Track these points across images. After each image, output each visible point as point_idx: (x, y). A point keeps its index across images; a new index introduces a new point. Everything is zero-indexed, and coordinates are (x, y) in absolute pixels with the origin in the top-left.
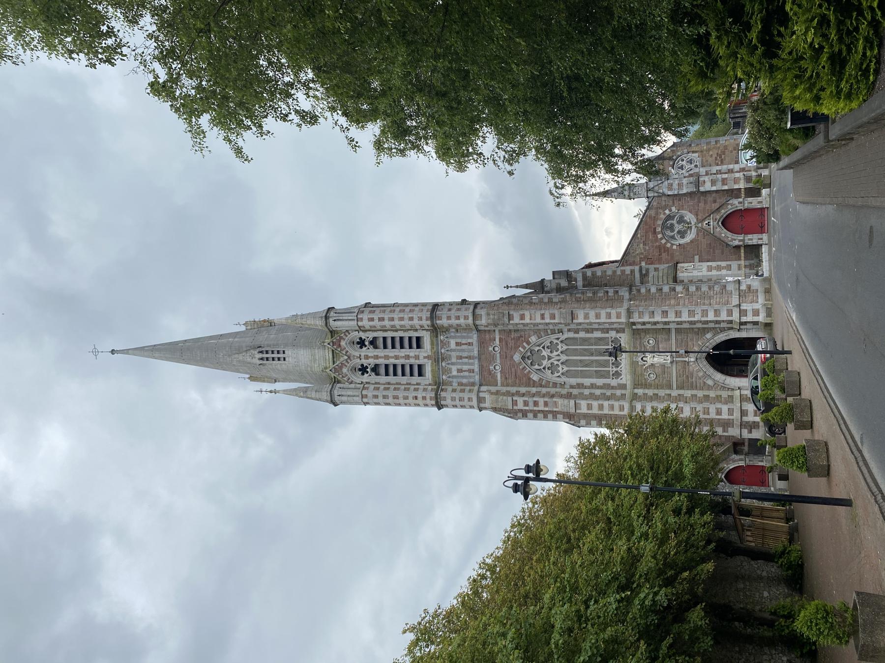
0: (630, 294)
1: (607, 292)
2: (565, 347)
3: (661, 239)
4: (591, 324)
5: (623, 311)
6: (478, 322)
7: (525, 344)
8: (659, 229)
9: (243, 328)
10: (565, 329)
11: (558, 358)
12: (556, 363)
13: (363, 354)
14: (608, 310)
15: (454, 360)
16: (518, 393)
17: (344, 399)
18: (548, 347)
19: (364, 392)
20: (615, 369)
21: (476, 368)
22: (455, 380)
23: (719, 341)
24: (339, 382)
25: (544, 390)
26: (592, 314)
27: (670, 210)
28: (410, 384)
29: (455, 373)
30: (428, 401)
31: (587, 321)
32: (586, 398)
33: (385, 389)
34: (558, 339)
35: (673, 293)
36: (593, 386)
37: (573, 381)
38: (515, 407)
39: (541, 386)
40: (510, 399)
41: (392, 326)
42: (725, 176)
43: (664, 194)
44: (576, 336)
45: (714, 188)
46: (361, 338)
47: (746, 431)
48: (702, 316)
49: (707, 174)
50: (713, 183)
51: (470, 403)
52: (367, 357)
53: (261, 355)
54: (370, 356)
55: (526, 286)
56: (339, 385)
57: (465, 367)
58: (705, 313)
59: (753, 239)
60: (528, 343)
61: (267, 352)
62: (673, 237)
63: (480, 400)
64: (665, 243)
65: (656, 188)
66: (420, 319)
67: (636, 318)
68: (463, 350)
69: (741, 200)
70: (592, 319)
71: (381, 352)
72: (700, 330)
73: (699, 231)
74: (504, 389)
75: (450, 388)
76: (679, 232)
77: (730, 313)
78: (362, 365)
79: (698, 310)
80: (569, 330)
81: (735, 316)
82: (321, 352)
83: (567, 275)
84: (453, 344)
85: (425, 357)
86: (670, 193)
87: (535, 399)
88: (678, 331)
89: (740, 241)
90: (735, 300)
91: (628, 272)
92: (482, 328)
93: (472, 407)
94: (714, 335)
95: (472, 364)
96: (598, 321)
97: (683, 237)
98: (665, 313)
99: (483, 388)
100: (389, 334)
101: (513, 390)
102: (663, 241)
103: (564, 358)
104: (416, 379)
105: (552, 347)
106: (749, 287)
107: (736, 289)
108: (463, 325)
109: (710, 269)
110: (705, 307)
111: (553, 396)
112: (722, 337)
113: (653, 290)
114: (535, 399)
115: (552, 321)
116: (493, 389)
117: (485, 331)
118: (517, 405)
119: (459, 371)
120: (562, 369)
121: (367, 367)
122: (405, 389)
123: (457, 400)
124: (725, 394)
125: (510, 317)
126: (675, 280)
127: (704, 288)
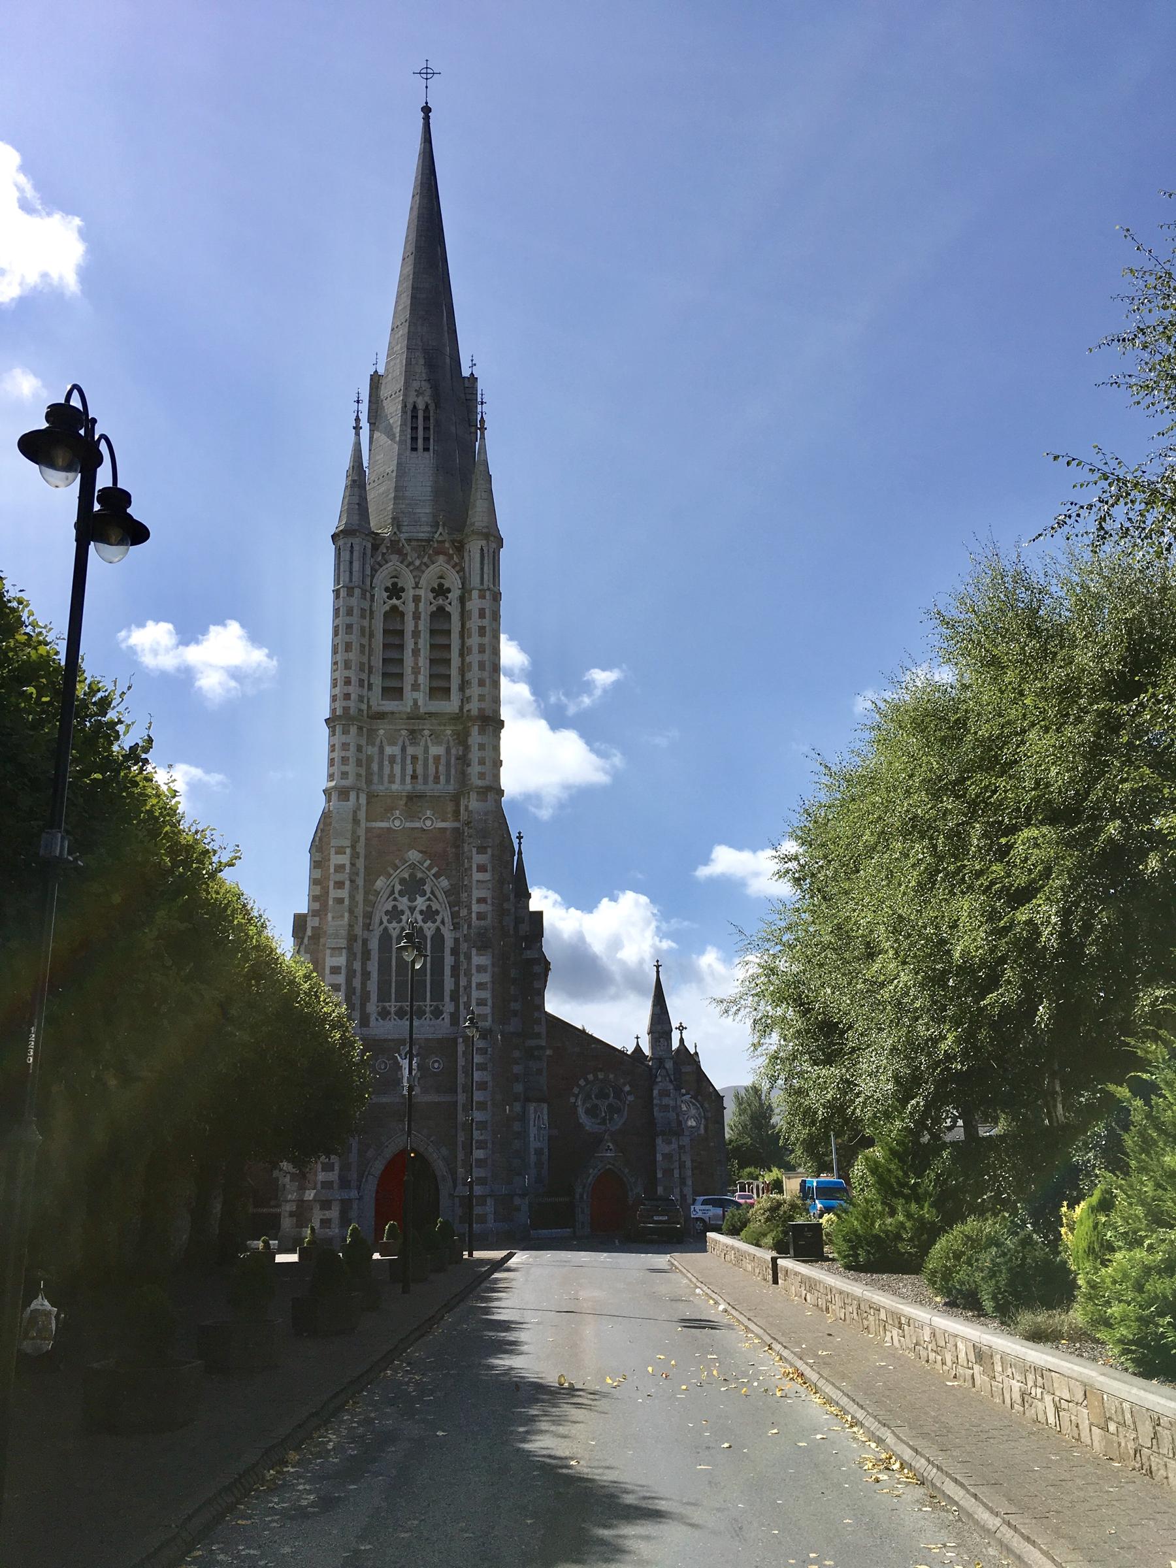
2: (429, 934)
3: (586, 1080)
4: (468, 974)
7: (428, 862)
9: (466, 373)
13: (422, 592)
14: (490, 1003)
16: (355, 856)
17: (346, 555)
18: (429, 907)
19: (357, 592)
20: (393, 1010)
22: (376, 749)
25: (360, 897)
26: (485, 978)
27: (629, 1093)
28: (370, 672)
29: (389, 750)
31: (474, 971)
33: (362, 629)
34: (443, 922)
36: (366, 975)
39: (366, 893)
40: (347, 843)
41: (470, 650)
42: (676, 1174)
43: (654, 1083)
44: (447, 951)
45: (659, 1157)
46: (449, 590)
47: (294, 1208)
49: (681, 1147)
50: (668, 1157)
52: (416, 599)
53: (421, 406)
60: (437, 876)
62: (588, 1097)
64: (579, 1086)
65: (664, 1072)
68: (426, 766)
75: (363, 742)
76: (596, 1106)
80: (456, 940)
85: (415, 702)
86: (655, 1092)
87: (347, 883)
89: (581, 1197)
91: (537, 1029)
92: (463, 802)
96: (474, 985)
97: (587, 1112)
102: (582, 1083)
108: (469, 770)
110: (490, 1145)
111: (351, 912)
113: (517, 1069)
115: (474, 916)
116: (362, 815)
118: (337, 853)
122: (362, 664)
123: (343, 754)
124: (353, 1176)
125: (482, 850)
126: (528, 1100)
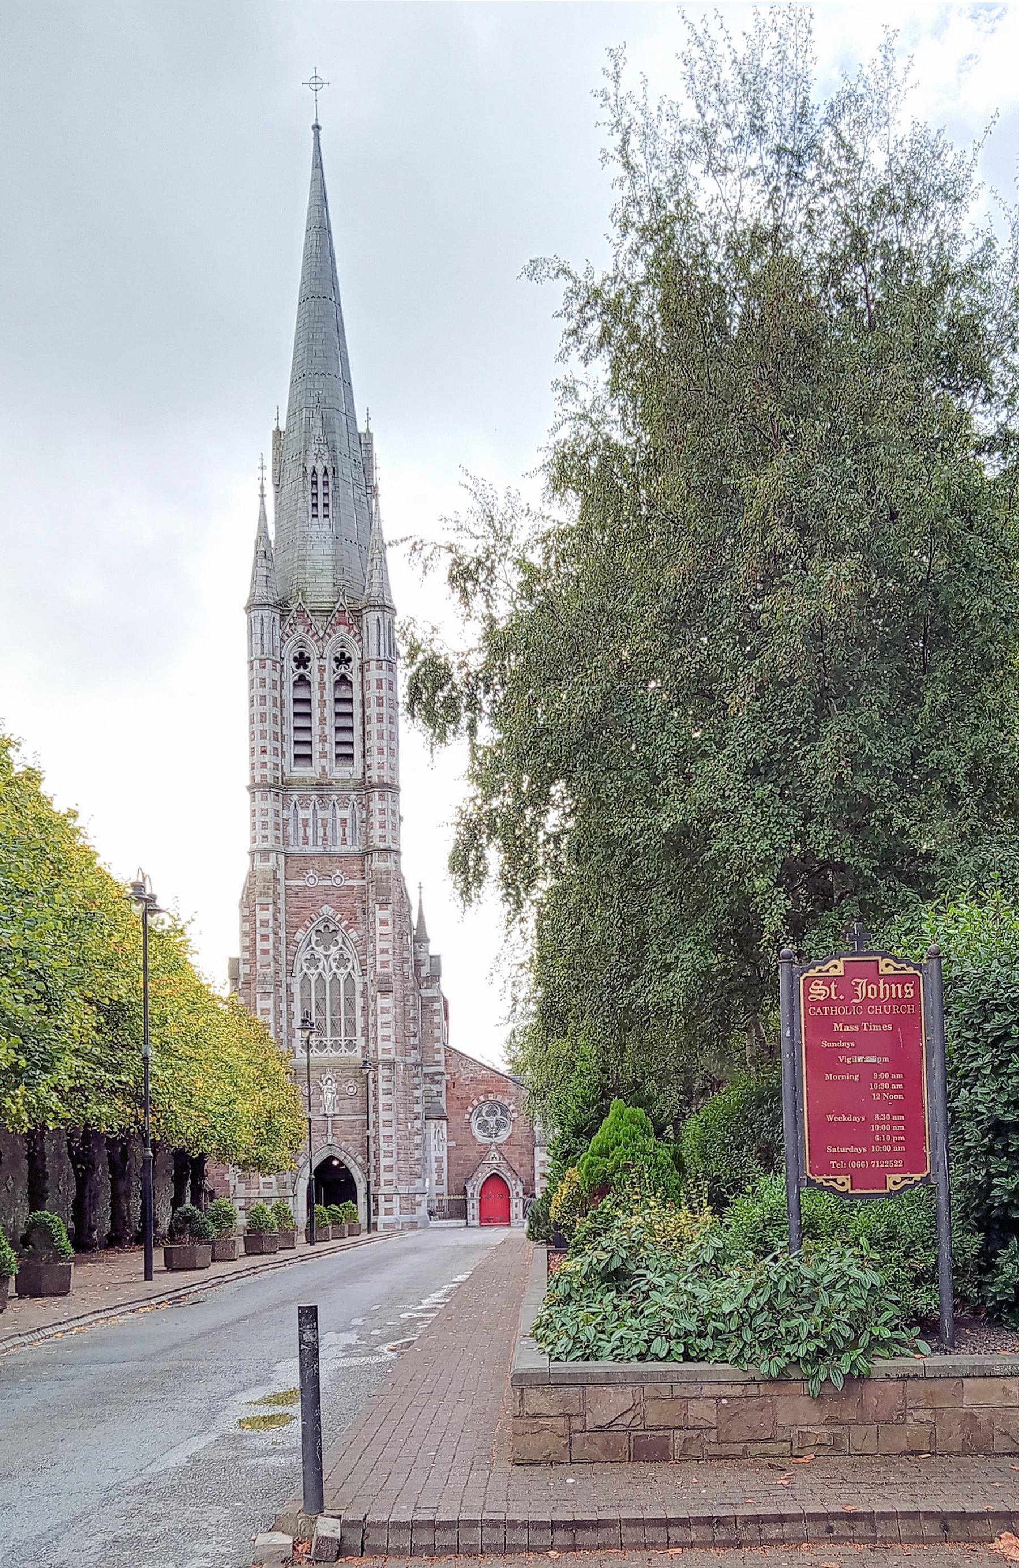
0: (413, 1064)
1: (415, 1036)
5: (391, 1056)
6: (375, 855)
7: (345, 922)
8: (490, 1097)
9: (361, 428)
10: (366, 979)
11: (327, 968)
12: (320, 965)
15: (321, 814)
16: (277, 911)
21: (309, 849)
23: (352, 1171)
24: (282, 618)
25: (282, 948)
26: (388, 1018)
29: (302, 814)
30: (258, 772)
32: (276, 1007)
35: (413, 1116)
37: (296, 989)
38: (258, 907)
40: (270, 900)
44: (358, 994)
45: (537, 1164)
48: (385, 1152)
51: (259, 838)
52: (322, 669)
53: (320, 472)
54: (322, 672)
55: (421, 917)
56: (278, 617)
57: (310, 832)
58: (389, 1154)
59: (474, 1210)
61: (326, 484)
63: (265, 854)
66: (381, 766)
67: (383, 1072)
68: (334, 829)
69: (521, 1195)
70: (382, 1018)
71: (329, 694)
72: (367, 1149)
73: (487, 1148)
74: (281, 890)
77: (389, 1183)
78: (308, 659)
79: (393, 1147)
80: (365, 985)
81: (385, 1189)
82: (330, 588)
83: (435, 976)
84: (344, 814)
87: (271, 936)
88: (366, 1124)
90: (402, 1189)
91: (437, 1057)
93: (254, 840)
94: (360, 1165)
95: (315, 844)
97: (479, 1127)
98: (389, 1107)
99: (281, 857)
100: (356, 708)
101: (281, 905)
103: (328, 977)
104: (291, 750)
105: (342, 961)
106: (419, 1204)
107: (416, 1189)
109: (439, 1160)
112: (357, 1174)
114: (271, 936)
116: (281, 875)
117: (363, 865)
118: (262, 909)
119: (305, 822)
120: (313, 973)
121: (306, 667)
123: (263, 819)
127: (418, 1154)
